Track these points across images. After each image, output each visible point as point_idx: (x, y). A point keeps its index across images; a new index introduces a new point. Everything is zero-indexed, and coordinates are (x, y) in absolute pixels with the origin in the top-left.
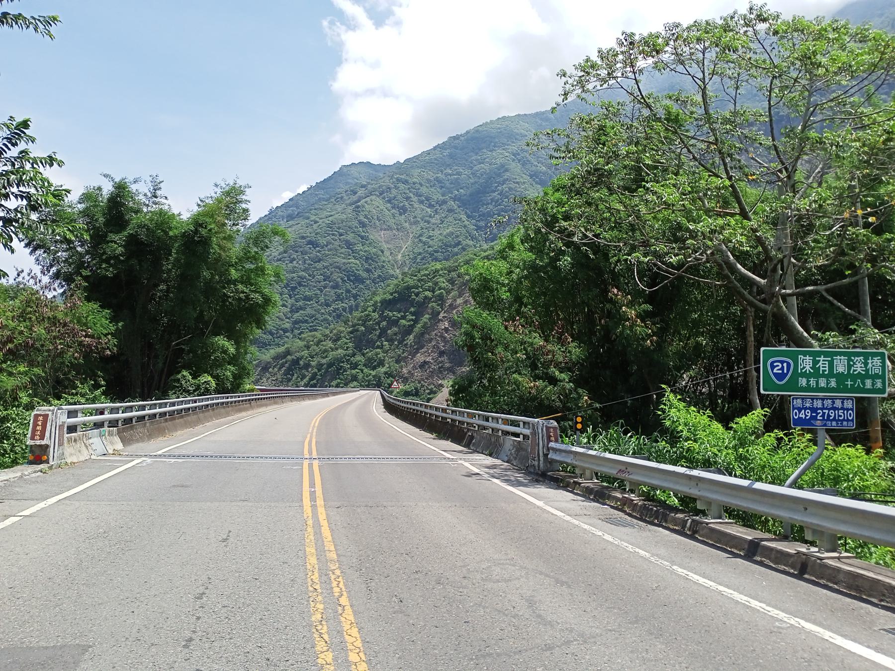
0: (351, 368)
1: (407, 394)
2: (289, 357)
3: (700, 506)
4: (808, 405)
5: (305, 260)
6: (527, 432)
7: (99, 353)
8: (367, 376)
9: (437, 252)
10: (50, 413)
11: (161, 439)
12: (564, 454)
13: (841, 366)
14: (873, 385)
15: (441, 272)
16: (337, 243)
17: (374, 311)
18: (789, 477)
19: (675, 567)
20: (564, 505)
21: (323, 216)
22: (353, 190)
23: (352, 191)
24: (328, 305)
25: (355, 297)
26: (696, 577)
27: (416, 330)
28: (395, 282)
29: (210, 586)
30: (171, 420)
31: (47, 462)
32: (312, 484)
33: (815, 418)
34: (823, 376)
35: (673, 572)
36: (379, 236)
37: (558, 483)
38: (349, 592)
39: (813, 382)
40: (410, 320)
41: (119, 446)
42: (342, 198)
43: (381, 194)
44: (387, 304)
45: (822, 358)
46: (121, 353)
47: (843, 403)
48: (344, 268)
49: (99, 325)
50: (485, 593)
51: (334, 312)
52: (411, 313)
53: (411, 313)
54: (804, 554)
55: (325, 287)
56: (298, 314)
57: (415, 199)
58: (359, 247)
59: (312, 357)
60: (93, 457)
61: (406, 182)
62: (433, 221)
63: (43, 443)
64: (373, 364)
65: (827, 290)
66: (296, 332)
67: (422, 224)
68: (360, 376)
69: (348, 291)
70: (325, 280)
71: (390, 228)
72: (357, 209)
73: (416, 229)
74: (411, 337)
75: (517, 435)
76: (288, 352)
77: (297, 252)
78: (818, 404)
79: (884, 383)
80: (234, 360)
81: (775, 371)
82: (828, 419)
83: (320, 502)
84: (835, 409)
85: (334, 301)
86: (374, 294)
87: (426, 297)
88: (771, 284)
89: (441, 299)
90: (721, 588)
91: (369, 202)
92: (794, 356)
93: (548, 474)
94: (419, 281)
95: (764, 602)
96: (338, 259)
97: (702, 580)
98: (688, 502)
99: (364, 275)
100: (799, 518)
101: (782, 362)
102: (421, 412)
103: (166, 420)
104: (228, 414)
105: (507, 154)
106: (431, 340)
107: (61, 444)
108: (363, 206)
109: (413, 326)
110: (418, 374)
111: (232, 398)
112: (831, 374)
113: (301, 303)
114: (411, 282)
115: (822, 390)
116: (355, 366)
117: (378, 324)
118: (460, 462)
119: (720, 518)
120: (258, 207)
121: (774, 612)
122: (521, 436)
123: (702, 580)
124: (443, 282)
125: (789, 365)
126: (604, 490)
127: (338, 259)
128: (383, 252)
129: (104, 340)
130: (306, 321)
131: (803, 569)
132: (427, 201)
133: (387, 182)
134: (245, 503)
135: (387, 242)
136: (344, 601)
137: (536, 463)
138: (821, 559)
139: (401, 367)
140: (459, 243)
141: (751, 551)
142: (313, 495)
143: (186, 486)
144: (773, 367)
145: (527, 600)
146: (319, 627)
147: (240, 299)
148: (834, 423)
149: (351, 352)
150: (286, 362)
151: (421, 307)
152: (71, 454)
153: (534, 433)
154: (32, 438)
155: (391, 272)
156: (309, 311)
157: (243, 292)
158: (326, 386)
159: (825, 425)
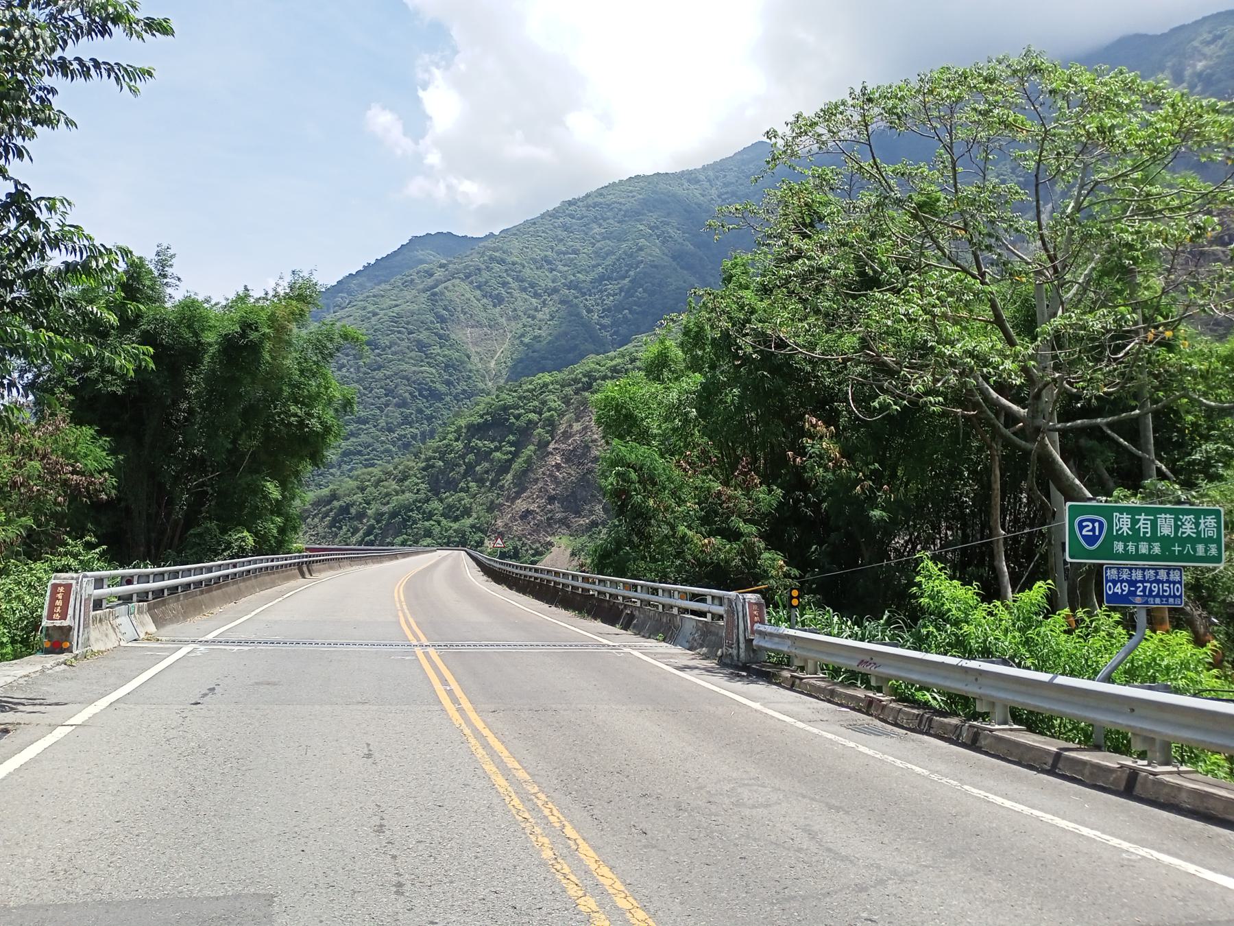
0: (424, 519)
1: (503, 555)
2: (336, 503)
3: (980, 708)
4: (1125, 577)
5: (359, 367)
6: (720, 610)
7: (90, 498)
8: (446, 531)
9: (546, 359)
10: (74, 582)
11: (197, 618)
12: (776, 640)
13: (1166, 529)
14: (1206, 551)
15: (551, 387)
16: (405, 344)
17: (457, 440)
18: (1097, 663)
19: (966, 787)
20: (788, 707)
21: (384, 306)
22: (431, 266)
23: (426, 272)
24: (391, 430)
25: (430, 419)
26: (999, 800)
27: (515, 466)
28: (487, 399)
29: (385, 816)
30: (208, 592)
31: (70, 650)
32: (444, 682)
33: (1133, 594)
34: (1144, 539)
35: (966, 793)
36: (464, 335)
37: (768, 677)
38: (571, 822)
39: (1131, 547)
40: (507, 453)
41: (152, 628)
42: (412, 280)
43: (467, 277)
44: (476, 430)
45: (1143, 517)
46: (119, 499)
47: (1168, 574)
48: (414, 378)
49: (92, 456)
50: (747, 822)
51: (399, 439)
52: (509, 442)
53: (509, 442)
54: (1130, 768)
55: (387, 405)
56: (348, 443)
57: (514, 285)
58: (436, 350)
59: (368, 504)
60: (123, 643)
61: (502, 262)
62: (540, 315)
63: (65, 623)
64: (452, 513)
65: (1109, 425)
66: (346, 467)
67: (525, 320)
68: (437, 530)
69: (420, 411)
70: (386, 395)
71: (479, 325)
72: (434, 298)
73: (516, 327)
74: (509, 477)
75: (702, 614)
76: (334, 496)
77: (347, 355)
78: (1138, 575)
79: (1219, 549)
80: (279, 508)
81: (1084, 533)
82: (1150, 595)
83: (466, 705)
84: (1158, 582)
85: (399, 425)
86: (457, 415)
87: (530, 421)
88: (1034, 414)
89: (551, 424)
90: (1036, 813)
91: (451, 288)
92: (1108, 513)
93: (754, 665)
94: (520, 398)
95: (1097, 829)
96: (405, 366)
97: (1008, 804)
98: (959, 703)
99: (443, 388)
100: (1122, 722)
101: (1093, 521)
102: (548, 581)
103: (202, 592)
104: (273, 585)
105: (642, 227)
106: (536, 481)
107: (86, 626)
108: (442, 293)
109: (510, 461)
110: (518, 528)
111: (279, 560)
112: (1154, 538)
113: (352, 427)
114: (510, 400)
115: (1201, 559)
116: (429, 516)
117: (463, 457)
118: (626, 650)
119: (1006, 723)
120: (257, 293)
121: (1114, 841)
122: (709, 615)
123: (1008, 804)
124: (554, 401)
125: (1101, 524)
126: (847, 683)
127: (405, 366)
128: (469, 357)
129: (98, 479)
130: (360, 453)
131: (1129, 787)
132: (531, 288)
133: (477, 260)
134: (366, 707)
135: (475, 344)
136: (570, 831)
137: (735, 652)
138: (1155, 774)
139: (495, 518)
140: (575, 347)
141: (1055, 766)
142: (450, 693)
143: (275, 684)
144: (1081, 528)
145: (804, 830)
146: (558, 867)
147: (290, 424)
148: (1158, 600)
149: (423, 496)
150: (331, 510)
151: (525, 433)
152: (97, 640)
153: (732, 611)
154: (50, 617)
155: (481, 385)
156: (363, 438)
157: (295, 415)
158: (389, 544)
159: (1146, 603)
